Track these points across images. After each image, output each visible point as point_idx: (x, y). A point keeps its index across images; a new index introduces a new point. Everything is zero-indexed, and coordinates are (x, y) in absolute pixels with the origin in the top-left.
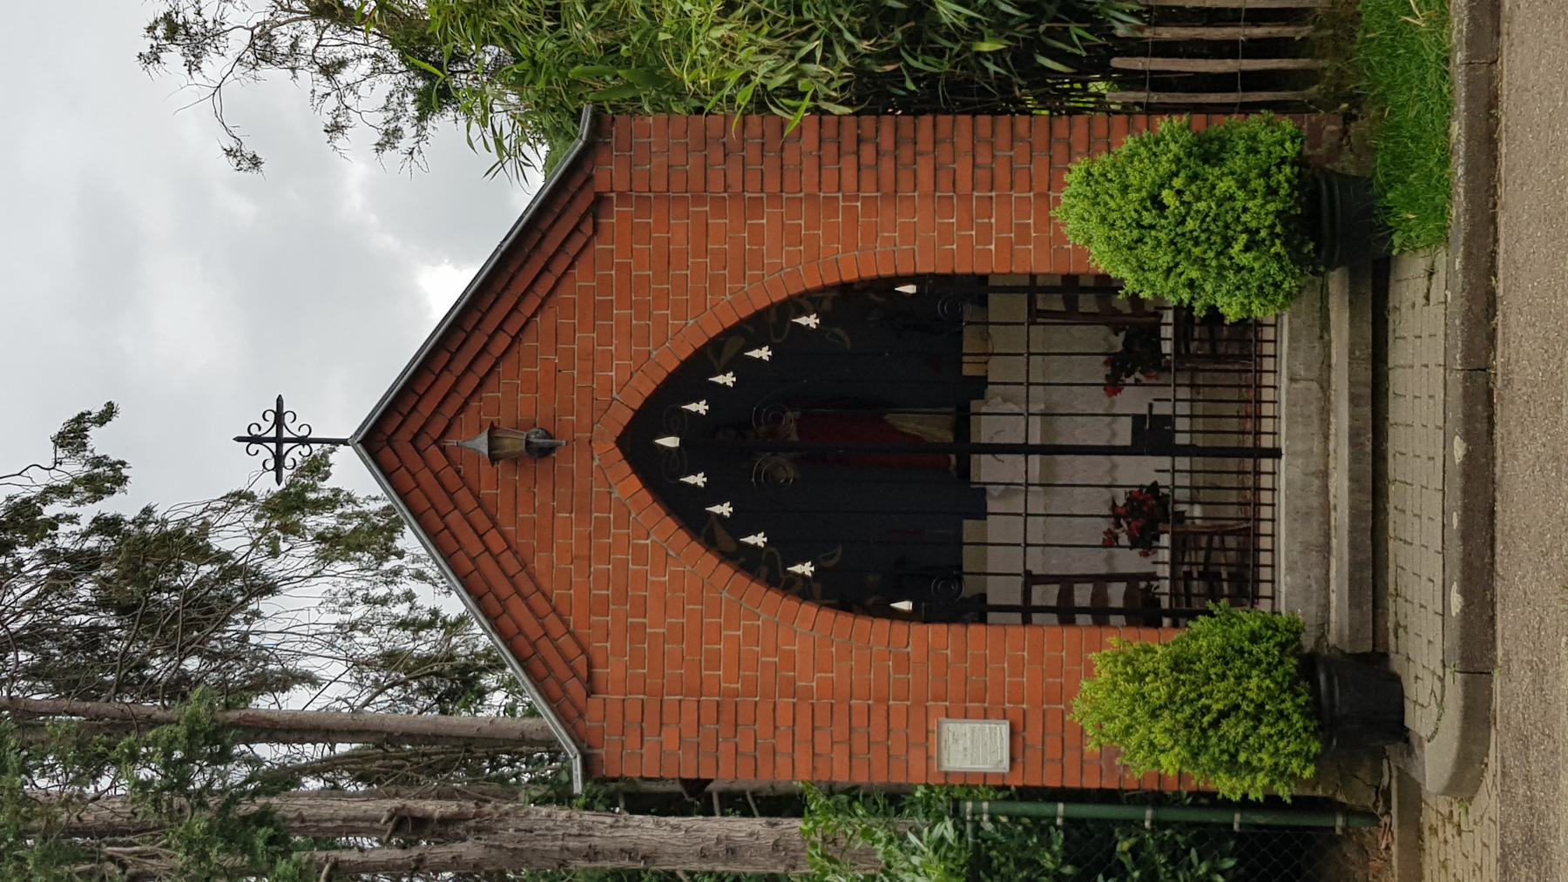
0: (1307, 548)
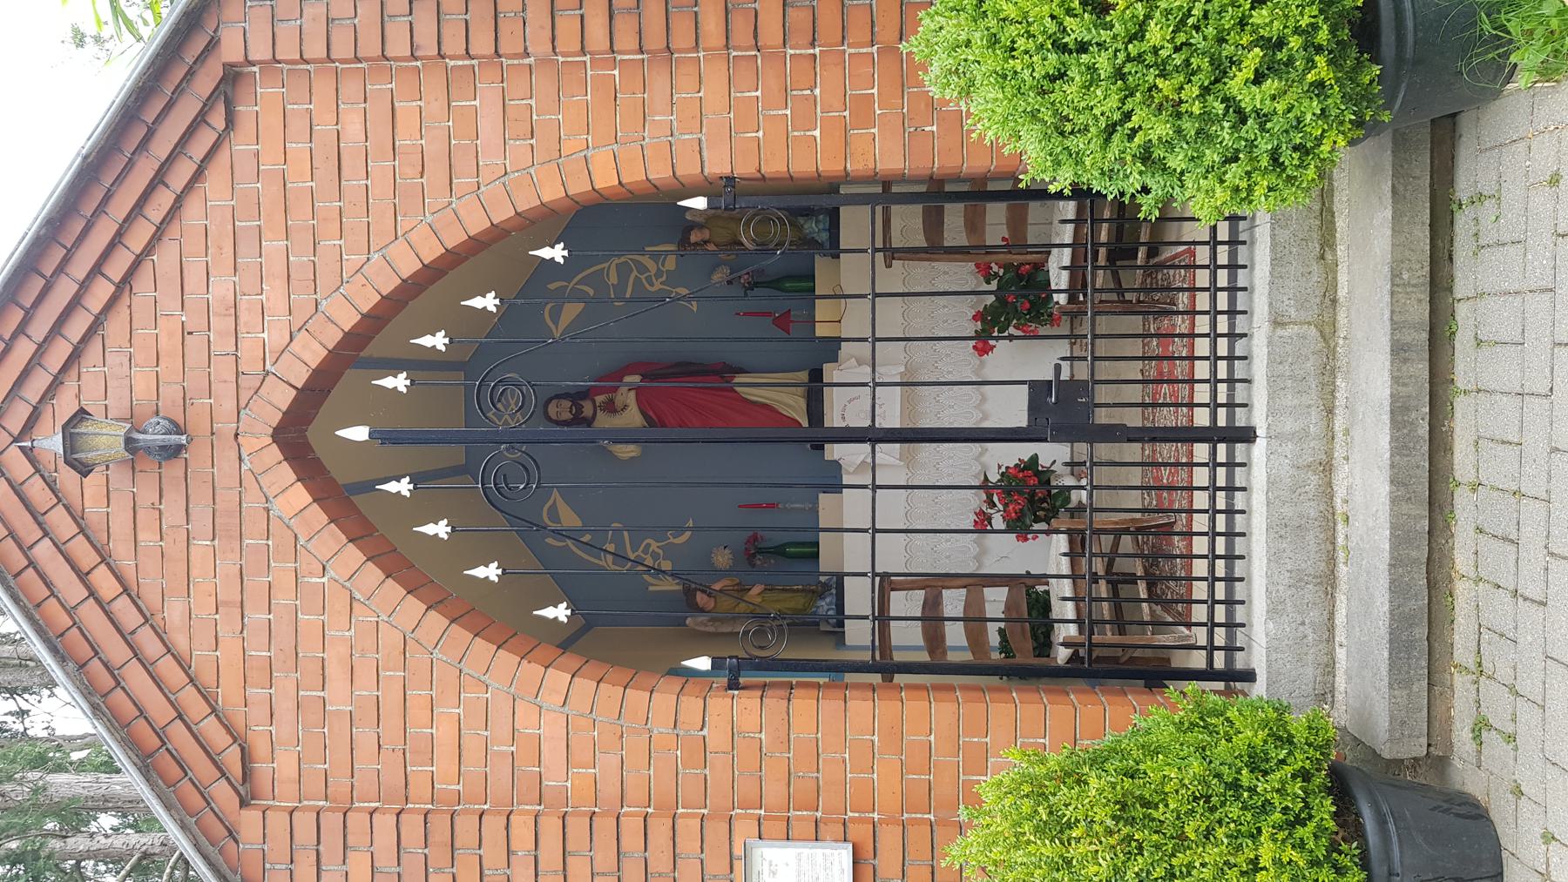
0: (1298, 581)
